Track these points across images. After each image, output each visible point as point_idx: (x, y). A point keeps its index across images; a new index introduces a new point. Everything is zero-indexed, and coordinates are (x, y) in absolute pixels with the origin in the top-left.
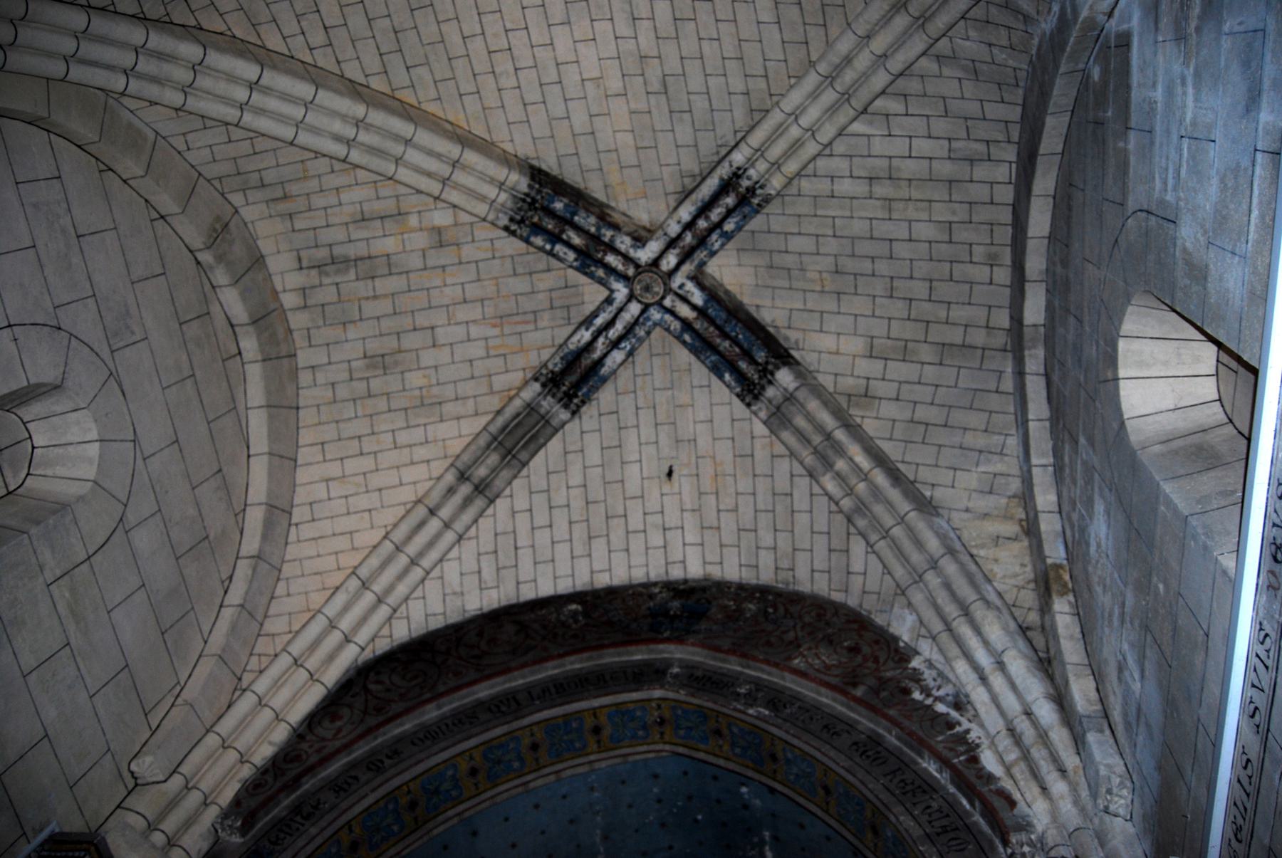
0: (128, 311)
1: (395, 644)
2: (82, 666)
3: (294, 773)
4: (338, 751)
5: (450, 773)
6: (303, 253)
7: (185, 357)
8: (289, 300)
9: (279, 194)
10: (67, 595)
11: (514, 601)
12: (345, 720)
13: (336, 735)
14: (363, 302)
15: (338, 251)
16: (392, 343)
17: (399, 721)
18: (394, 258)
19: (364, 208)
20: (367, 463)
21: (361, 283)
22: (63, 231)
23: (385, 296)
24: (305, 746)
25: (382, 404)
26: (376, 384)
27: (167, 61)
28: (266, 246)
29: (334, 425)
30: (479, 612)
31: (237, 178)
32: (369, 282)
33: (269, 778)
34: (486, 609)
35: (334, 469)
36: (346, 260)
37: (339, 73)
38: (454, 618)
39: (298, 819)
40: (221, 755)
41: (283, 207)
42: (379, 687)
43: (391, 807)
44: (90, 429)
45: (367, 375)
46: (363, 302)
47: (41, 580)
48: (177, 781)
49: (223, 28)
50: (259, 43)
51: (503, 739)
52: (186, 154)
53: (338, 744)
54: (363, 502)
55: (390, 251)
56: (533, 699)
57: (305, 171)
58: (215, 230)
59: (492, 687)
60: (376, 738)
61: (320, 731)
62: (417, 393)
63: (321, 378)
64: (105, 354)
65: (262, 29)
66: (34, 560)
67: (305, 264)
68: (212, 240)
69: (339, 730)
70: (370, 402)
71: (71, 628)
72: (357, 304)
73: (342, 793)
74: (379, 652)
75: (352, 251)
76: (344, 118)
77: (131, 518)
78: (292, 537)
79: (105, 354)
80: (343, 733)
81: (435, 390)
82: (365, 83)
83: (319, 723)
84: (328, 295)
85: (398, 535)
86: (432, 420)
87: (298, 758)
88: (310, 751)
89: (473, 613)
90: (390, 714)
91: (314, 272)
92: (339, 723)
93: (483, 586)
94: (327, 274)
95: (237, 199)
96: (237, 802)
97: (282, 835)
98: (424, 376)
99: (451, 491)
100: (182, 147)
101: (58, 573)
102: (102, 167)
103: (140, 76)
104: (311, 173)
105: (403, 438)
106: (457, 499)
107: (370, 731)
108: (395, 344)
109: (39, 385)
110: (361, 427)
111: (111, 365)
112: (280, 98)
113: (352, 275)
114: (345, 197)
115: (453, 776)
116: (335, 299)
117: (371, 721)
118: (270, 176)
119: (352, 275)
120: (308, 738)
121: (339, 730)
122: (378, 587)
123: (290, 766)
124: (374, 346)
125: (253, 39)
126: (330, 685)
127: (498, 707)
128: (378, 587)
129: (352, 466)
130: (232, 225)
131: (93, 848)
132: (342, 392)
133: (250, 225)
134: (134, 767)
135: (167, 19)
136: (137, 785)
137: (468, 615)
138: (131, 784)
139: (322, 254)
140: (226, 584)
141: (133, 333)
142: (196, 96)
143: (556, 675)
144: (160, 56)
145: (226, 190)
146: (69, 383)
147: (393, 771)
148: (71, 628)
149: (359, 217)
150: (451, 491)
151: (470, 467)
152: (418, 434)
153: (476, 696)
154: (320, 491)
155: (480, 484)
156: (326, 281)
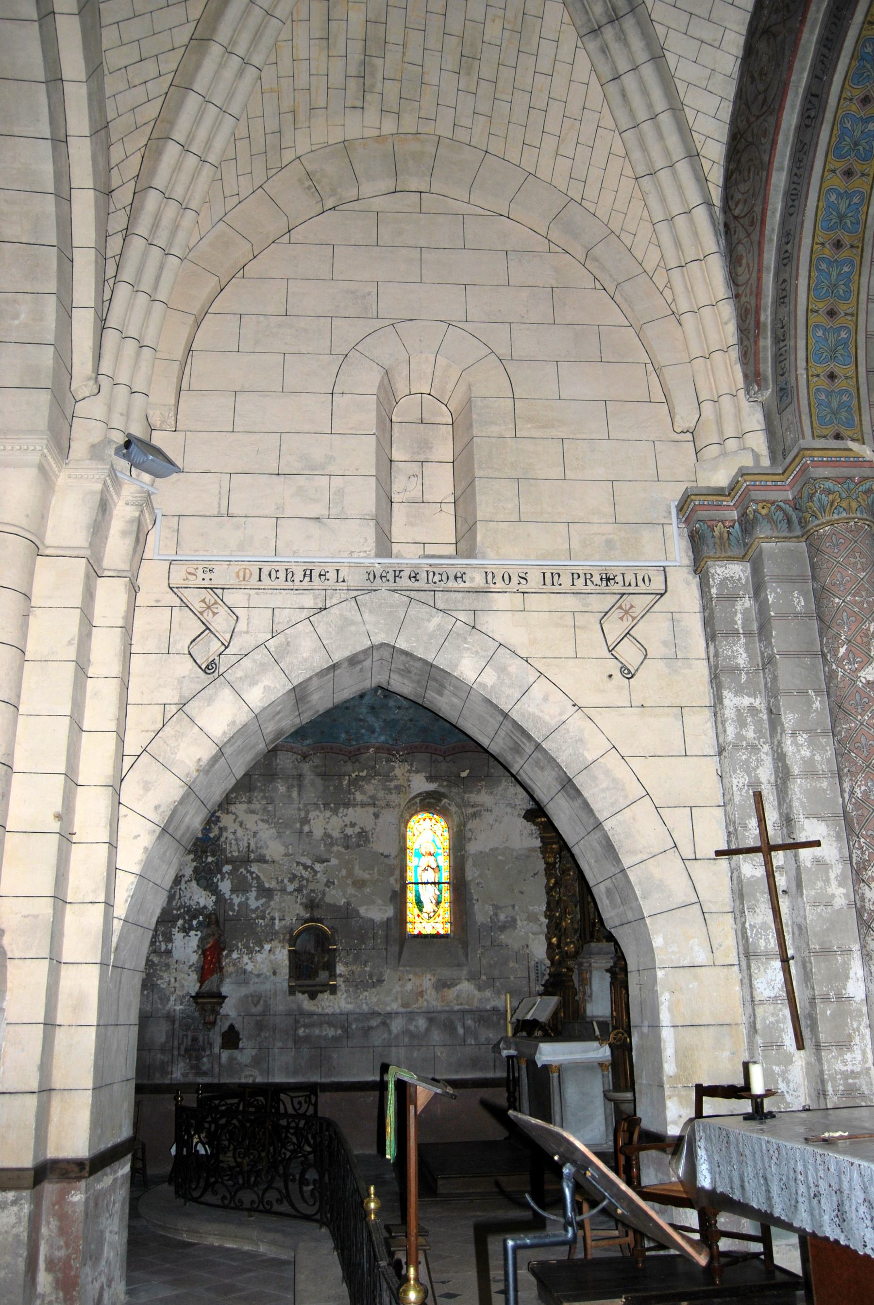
0: (353, 292)
1: (722, 163)
2: (584, 436)
3: (752, 323)
4: (759, 279)
5: (833, 198)
6: (348, 104)
7: (404, 251)
8: (389, 126)
9: (290, 116)
10: (529, 426)
11: (748, 17)
12: (744, 254)
13: (749, 270)
14: (406, 60)
15: (353, 70)
16: (452, 43)
17: (769, 213)
18: (371, 16)
19: (317, 36)
20: (556, 109)
21: (388, 55)
22: (279, 326)
23: (405, 35)
24: (743, 299)
25: (506, 73)
26: (487, 72)
27: (159, 220)
28: (336, 136)
29: (511, 125)
30: (739, 61)
31: (269, 154)
32: (388, 47)
33: (746, 343)
34: (740, 53)
35: (550, 143)
36: (364, 64)
37: (173, 74)
38: (731, 90)
39: (782, 344)
40: (711, 364)
41: (302, 116)
42: (740, 206)
43: (824, 266)
44: (426, 358)
45: (476, 78)
46: (406, 60)
47: (509, 440)
48: (707, 407)
49: (138, 156)
50: (152, 123)
51: (835, 132)
52: (242, 197)
53: (754, 275)
54: (588, 129)
55: (363, 18)
56: (821, 79)
57: (272, 91)
58: (309, 188)
59: (793, 107)
60: (771, 240)
61: (741, 280)
62: (507, 34)
63: (465, 121)
64: (377, 324)
65: (140, 121)
66: (493, 440)
67: (360, 104)
68: (317, 194)
69: (748, 265)
70: (500, 84)
71: (554, 433)
72: (406, 65)
73: (786, 300)
74: (721, 182)
75: (356, 57)
76: (222, 65)
77: (503, 351)
78: (592, 208)
79: (377, 324)
80: (751, 265)
81: (510, 14)
82: (195, 22)
83: (737, 275)
84: (392, 90)
85: (625, 122)
86: (538, 29)
87: (747, 311)
88: (747, 299)
89: (737, 68)
90: (759, 218)
91: (368, 97)
92: (744, 261)
93: (717, 44)
94: (373, 86)
95: (288, 156)
96: (746, 376)
97: (782, 364)
98: (494, 21)
99: (604, 50)
100: (236, 200)
101: (512, 426)
102: (240, 274)
103: (170, 243)
104: (275, 86)
105: (545, 65)
106: (615, 47)
107: (760, 244)
108: (455, 40)
109: (381, 386)
110: (521, 99)
111: (387, 322)
112: (198, 125)
113: (379, 62)
114: (302, 54)
115: (840, 195)
116: (398, 84)
117: (755, 237)
118: (272, 126)
119: (379, 62)
120: (740, 292)
121: (748, 265)
122: (660, 163)
123: (748, 321)
124: (451, 62)
125: (148, 129)
126: (714, 248)
127: (809, 117)
128: (660, 163)
129: (552, 126)
130: (309, 168)
131: (693, 497)
132: (484, 107)
133: (314, 148)
134: (679, 430)
135: (128, 209)
136: (692, 433)
137: (736, 76)
138: (689, 436)
139: (352, 84)
140: (598, 285)
141: (369, 294)
142: (189, 200)
143: (819, 34)
144: (155, 225)
145: (279, 165)
146: (387, 364)
147: (796, 249)
148: (554, 433)
149: (325, 43)
150: (604, 50)
151: (589, 20)
152: (547, 48)
153: (793, 127)
154: (563, 164)
155: (610, 16)
156: (378, 88)
